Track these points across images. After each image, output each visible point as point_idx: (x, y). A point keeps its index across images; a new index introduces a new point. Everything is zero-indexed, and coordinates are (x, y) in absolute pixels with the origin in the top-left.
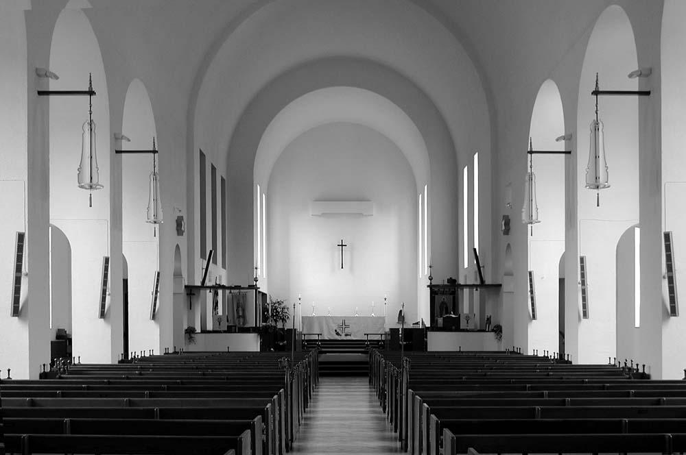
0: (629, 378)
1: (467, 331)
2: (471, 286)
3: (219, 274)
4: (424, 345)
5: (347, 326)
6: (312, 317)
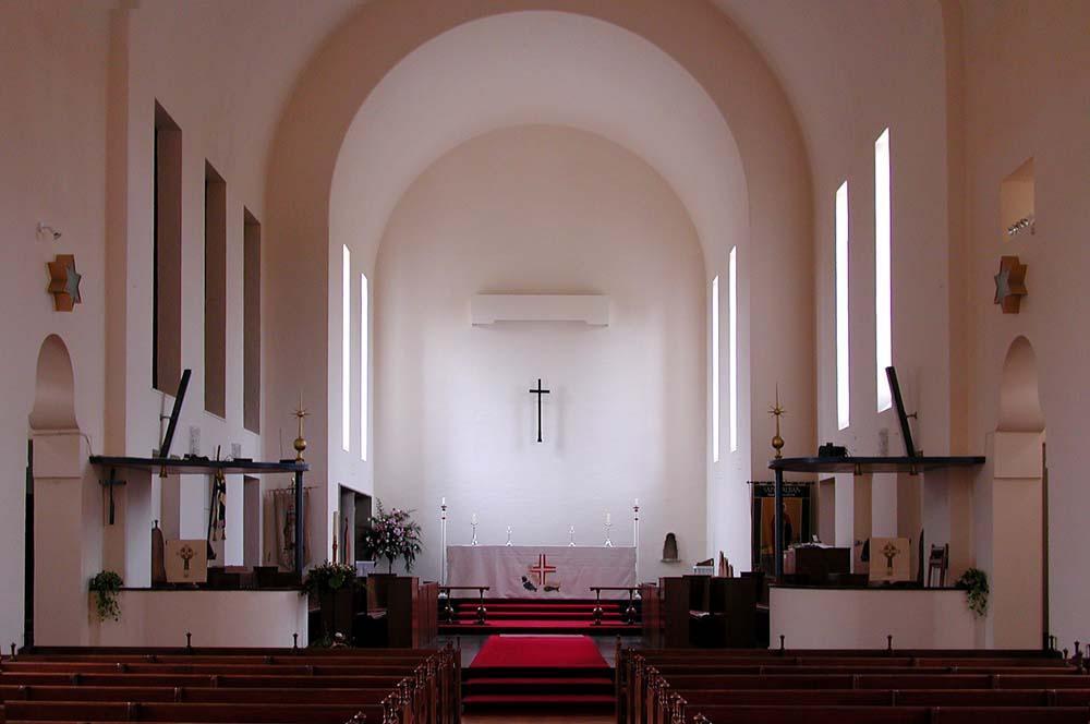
0: (1079, 672)
1: (887, 586)
2: (863, 467)
3: (236, 438)
4: (760, 624)
5: (551, 569)
6: (471, 549)
